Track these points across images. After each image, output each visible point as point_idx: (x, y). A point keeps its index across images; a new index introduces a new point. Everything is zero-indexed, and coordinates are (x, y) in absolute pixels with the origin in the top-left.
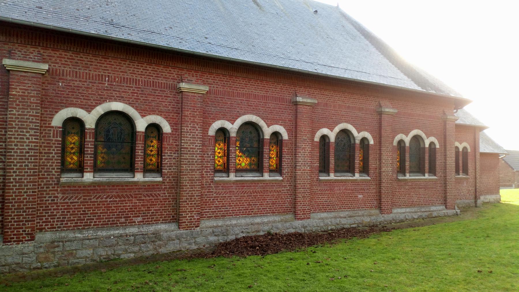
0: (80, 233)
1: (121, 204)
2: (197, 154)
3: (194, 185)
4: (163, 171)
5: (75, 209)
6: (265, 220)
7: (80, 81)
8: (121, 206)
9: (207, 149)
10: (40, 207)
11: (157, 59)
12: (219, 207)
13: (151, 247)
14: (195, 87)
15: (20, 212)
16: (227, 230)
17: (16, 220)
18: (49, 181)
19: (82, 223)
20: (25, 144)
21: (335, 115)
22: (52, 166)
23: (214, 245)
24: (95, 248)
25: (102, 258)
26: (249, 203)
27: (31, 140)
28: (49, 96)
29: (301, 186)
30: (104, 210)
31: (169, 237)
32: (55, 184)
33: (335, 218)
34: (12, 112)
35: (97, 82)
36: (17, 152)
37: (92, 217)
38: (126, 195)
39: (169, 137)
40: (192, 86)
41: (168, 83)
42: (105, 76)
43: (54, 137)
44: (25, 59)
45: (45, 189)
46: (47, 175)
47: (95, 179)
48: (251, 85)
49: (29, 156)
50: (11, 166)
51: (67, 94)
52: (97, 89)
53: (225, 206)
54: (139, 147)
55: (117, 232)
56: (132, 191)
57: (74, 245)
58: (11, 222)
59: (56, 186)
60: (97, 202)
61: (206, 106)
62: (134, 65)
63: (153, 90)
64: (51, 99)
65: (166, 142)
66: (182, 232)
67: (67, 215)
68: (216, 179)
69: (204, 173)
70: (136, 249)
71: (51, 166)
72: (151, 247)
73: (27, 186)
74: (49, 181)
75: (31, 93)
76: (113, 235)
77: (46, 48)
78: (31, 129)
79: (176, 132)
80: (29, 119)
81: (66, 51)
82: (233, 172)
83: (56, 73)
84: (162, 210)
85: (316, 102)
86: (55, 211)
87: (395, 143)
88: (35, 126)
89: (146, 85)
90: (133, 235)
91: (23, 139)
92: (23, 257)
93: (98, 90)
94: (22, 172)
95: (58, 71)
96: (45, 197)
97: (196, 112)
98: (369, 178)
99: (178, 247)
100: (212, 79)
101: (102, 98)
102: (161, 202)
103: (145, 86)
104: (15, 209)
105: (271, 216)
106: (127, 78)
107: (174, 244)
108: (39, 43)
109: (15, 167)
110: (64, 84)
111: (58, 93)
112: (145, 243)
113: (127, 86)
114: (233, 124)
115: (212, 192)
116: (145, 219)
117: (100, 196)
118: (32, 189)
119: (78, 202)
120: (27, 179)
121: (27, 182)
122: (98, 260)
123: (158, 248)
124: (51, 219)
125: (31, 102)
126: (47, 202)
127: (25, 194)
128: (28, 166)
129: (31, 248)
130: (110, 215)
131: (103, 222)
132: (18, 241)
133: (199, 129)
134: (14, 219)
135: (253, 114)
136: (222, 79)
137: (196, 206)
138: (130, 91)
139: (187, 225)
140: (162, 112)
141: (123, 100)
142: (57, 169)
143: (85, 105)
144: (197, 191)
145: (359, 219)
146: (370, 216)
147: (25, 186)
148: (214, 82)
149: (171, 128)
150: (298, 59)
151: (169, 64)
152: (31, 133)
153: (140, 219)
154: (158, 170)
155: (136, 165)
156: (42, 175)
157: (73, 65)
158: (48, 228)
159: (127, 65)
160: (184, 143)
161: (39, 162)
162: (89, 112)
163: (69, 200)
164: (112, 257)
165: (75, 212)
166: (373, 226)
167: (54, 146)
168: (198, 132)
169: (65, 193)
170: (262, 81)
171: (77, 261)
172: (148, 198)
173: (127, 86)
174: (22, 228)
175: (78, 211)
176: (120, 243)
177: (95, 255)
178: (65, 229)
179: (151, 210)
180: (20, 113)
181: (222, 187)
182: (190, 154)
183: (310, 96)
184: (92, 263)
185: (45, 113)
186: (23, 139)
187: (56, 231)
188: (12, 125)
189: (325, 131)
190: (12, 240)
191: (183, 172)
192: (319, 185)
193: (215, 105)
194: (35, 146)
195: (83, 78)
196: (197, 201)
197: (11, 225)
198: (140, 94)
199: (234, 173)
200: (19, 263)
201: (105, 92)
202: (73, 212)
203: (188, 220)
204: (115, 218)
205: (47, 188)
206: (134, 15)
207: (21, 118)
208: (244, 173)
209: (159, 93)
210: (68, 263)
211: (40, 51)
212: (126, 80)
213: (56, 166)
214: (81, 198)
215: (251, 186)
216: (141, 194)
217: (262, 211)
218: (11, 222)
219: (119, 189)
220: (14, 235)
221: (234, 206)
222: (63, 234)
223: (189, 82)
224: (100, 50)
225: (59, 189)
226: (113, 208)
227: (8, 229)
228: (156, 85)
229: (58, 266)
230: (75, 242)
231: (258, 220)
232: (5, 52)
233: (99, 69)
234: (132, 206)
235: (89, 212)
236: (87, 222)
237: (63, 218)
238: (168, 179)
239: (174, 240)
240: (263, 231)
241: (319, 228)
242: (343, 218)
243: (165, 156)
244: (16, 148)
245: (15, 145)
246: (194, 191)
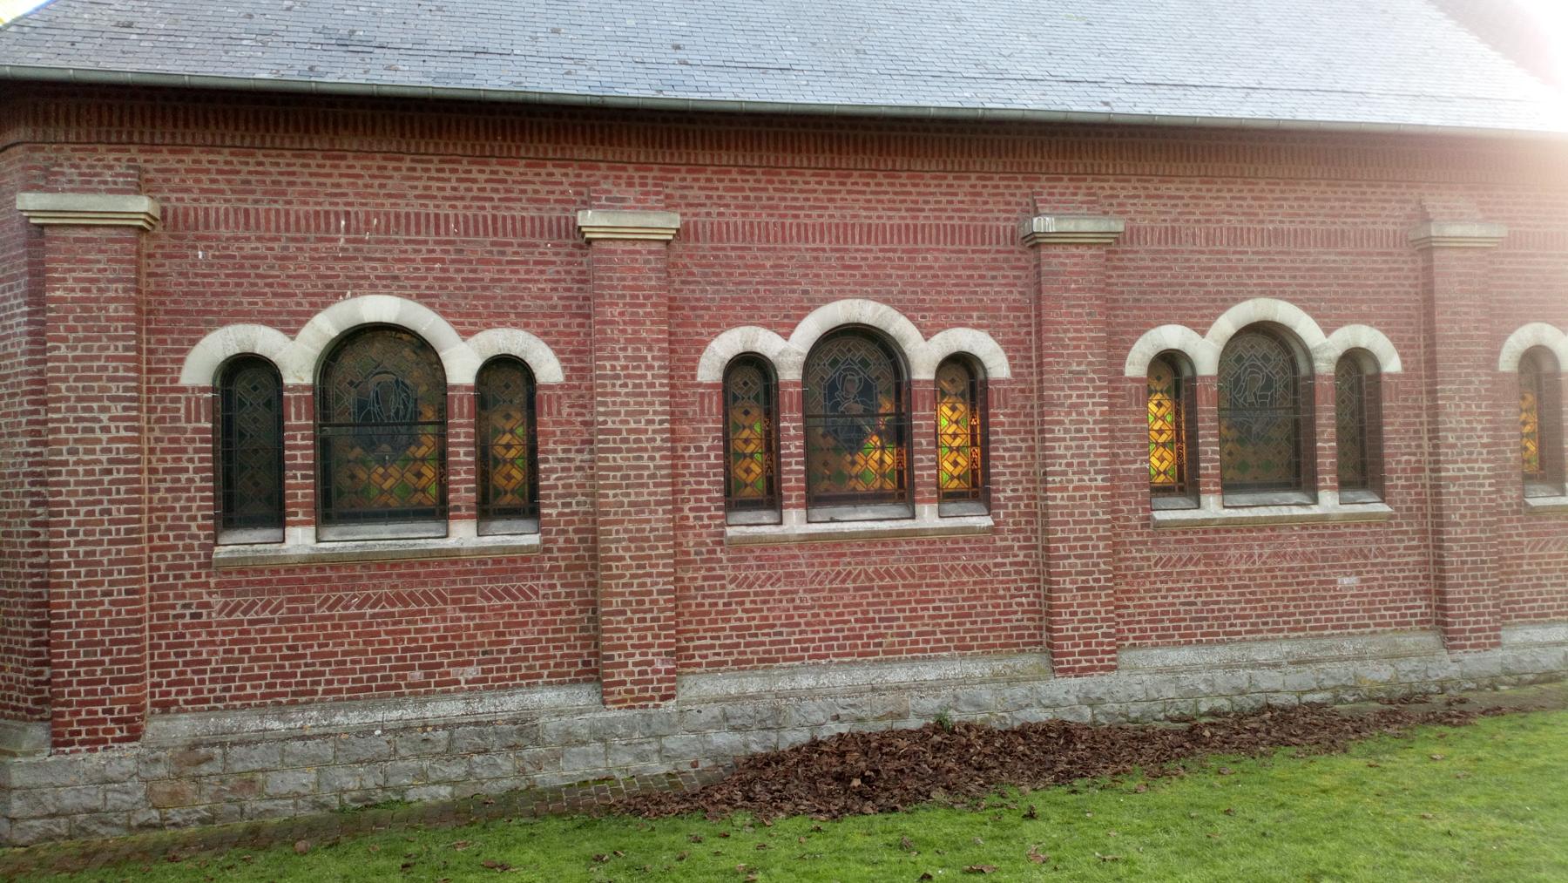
1: (408, 622)
2: (654, 449)
3: (649, 557)
4: (544, 511)
5: (263, 640)
6: (929, 673)
7: (259, 239)
8: (408, 632)
11: (504, 139)
12: (749, 628)
13: (506, 764)
14: (629, 220)
15: (95, 654)
17: (83, 677)
18: (182, 557)
19: (289, 685)
20: (98, 447)
21: (1213, 269)
22: (189, 509)
24: (322, 765)
25: (345, 797)
26: (865, 612)
27: (114, 433)
28: (170, 294)
29: (1072, 548)
32: (200, 566)
33: (1231, 666)
34: (56, 353)
35: (312, 236)
36: (75, 473)
37: (318, 668)
38: (424, 593)
39: (559, 397)
40: (627, 216)
41: (546, 216)
43: (188, 420)
44: (86, 187)
45: (171, 581)
46: (177, 538)
48: (849, 192)
49: (111, 482)
51: (223, 285)
52: (312, 259)
53: (773, 626)
55: (395, 714)
56: (444, 580)
57: (255, 759)
58: (69, 683)
59: (203, 572)
60: (332, 617)
62: (427, 170)
63: (493, 244)
64: (175, 302)
65: (550, 414)
66: (610, 715)
67: (242, 660)
68: (731, 532)
69: (686, 512)
70: (457, 770)
71: (183, 509)
72: (507, 766)
73: (110, 573)
74: (182, 557)
75: (107, 290)
76: (381, 725)
80: (105, 368)
81: (211, 147)
82: (797, 506)
83: (186, 221)
86: (204, 650)
87: (1507, 362)
88: (126, 389)
89: (471, 231)
90: (444, 727)
91: (92, 430)
92: (106, 791)
93: (316, 264)
94: (93, 533)
95: (192, 213)
96: (173, 607)
97: (643, 305)
98: (1384, 508)
100: (700, 188)
101: (330, 286)
102: (543, 614)
103: (467, 233)
104: (79, 645)
105: (953, 658)
106: (408, 215)
107: (587, 755)
108: (130, 134)
109: (73, 519)
110: (211, 253)
111: (196, 284)
112: (486, 751)
113: (407, 242)
114: (786, 336)
115: (723, 577)
116: (491, 671)
117: (340, 599)
118: (125, 582)
119: (272, 621)
120: (108, 552)
121: (111, 562)
122: (335, 804)
123: (529, 768)
124: (194, 672)
125: (108, 319)
127: (107, 599)
128: (109, 512)
129: (130, 765)
130: (374, 661)
131: (354, 681)
132: (93, 743)
133: (656, 364)
134: (78, 674)
136: (739, 184)
137: (660, 628)
138: (419, 257)
139: (631, 692)
140: (528, 316)
142: (204, 517)
143: (280, 313)
144: (660, 575)
145: (1339, 672)
146: (1393, 657)
147: (105, 573)
148: (709, 197)
150: (1036, 74)
151: (546, 152)
152: (114, 413)
153: (472, 672)
154: (528, 507)
155: (451, 496)
156: (161, 538)
157: (234, 192)
158: (186, 702)
159: (404, 173)
160: (605, 414)
161: (151, 501)
162: (292, 333)
163: (245, 613)
164: (379, 796)
166: (1406, 700)
167: (190, 448)
168: (655, 375)
169: (230, 594)
170: (892, 173)
171: (269, 805)
172: (496, 603)
176: (403, 752)
177: (326, 789)
178: (238, 703)
179: (510, 642)
180: (78, 353)
181: (758, 558)
182: (629, 450)
183: (1094, 206)
184: (318, 813)
186: (92, 430)
187: (210, 709)
188: (58, 390)
189: (1171, 336)
192: (1155, 542)
194: (127, 451)
195: (268, 229)
196: (662, 610)
198: (453, 261)
199: (802, 511)
200: (96, 810)
201: (338, 266)
202: (257, 650)
203: (632, 673)
204: (393, 669)
205: (176, 577)
207: (84, 369)
208: (844, 509)
210: (242, 812)
211: (134, 160)
212: (403, 221)
213: (199, 508)
214: (280, 606)
215: (867, 554)
216: (473, 591)
217: (916, 642)
218: (69, 683)
219: (400, 576)
221: (808, 624)
222: (228, 722)
223: (615, 203)
225: (212, 581)
226: (384, 637)
227: (63, 705)
229: (212, 820)
231: (900, 674)
232: (34, 172)
233: (316, 194)
234: (446, 629)
235: (308, 652)
236: (304, 684)
237: (229, 670)
238: (561, 539)
239: (584, 743)
240: (920, 716)
241: (1159, 707)
242: (1272, 668)
243: (546, 461)
244: (72, 459)
245: (72, 452)
246: (650, 575)
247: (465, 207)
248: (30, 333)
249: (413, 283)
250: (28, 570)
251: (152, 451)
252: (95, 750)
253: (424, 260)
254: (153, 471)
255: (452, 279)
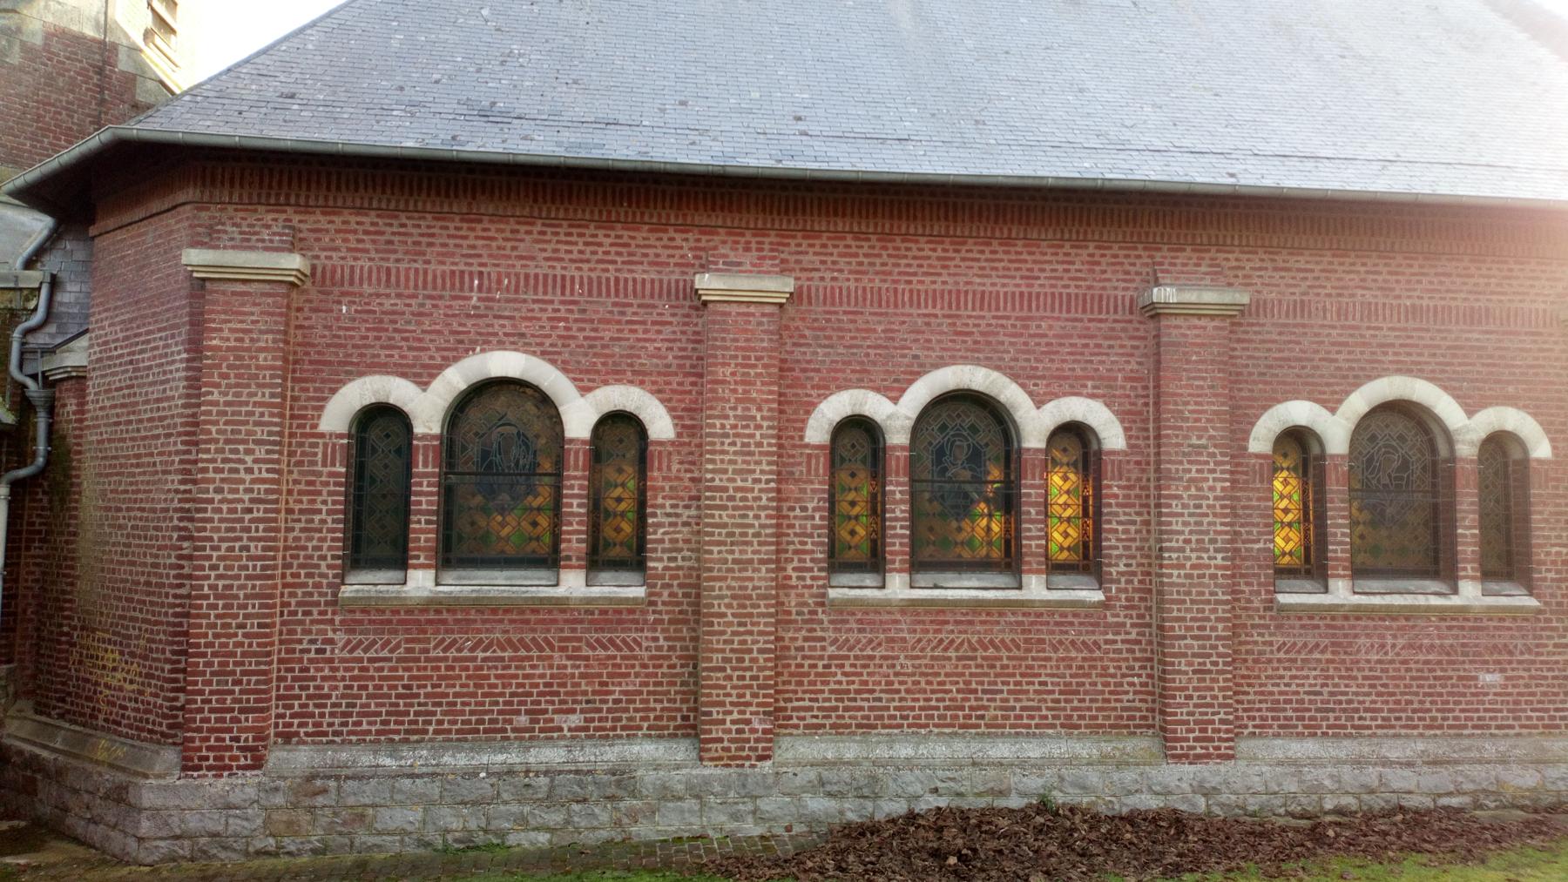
0: (391, 756)
1: (517, 668)
2: (760, 508)
3: (751, 615)
4: (651, 564)
5: (381, 678)
6: (1033, 750)
7: (399, 296)
8: (516, 676)
9: (803, 491)
10: (287, 670)
12: (848, 692)
13: (604, 815)
15: (218, 683)
16: (874, 779)
17: (214, 704)
18: (311, 594)
19: (402, 723)
20: (241, 487)
22: (319, 548)
23: (824, 829)
24: (429, 804)
25: (449, 837)
26: (967, 683)
27: (256, 475)
28: (313, 345)
29: (1188, 629)
30: (467, 686)
31: (665, 788)
32: (327, 604)
33: (1359, 762)
35: (447, 293)
36: (220, 510)
37: (430, 708)
39: (670, 453)
40: (742, 279)
41: (665, 278)
42: (471, 273)
43: (324, 464)
44: (245, 245)
45: (300, 616)
47: (440, 588)
48: (963, 259)
50: (204, 548)
52: (446, 315)
54: (572, 487)
55: (500, 758)
57: (367, 793)
58: (201, 710)
59: (330, 610)
60: (446, 659)
61: (795, 344)
62: (557, 234)
63: (615, 304)
64: (319, 353)
65: (660, 469)
66: (707, 772)
69: (790, 572)
70: (555, 818)
71: (316, 548)
72: (604, 817)
73: (245, 607)
74: (311, 594)
75: (258, 340)
76: (486, 768)
77: (306, 209)
78: (258, 442)
79: (693, 435)
80: (253, 414)
81: (360, 210)
82: (900, 571)
83: (333, 278)
84: (649, 693)
85: (1245, 299)
86: (326, 685)
90: (546, 773)
91: (237, 471)
93: (449, 320)
96: (300, 642)
97: (754, 366)
98: (1532, 602)
99: (696, 825)
100: (815, 254)
101: (461, 342)
102: (644, 666)
103: (590, 294)
104: (212, 674)
105: (1059, 736)
106: (536, 276)
107: (682, 812)
109: (215, 554)
110: (353, 308)
111: (339, 337)
112: (585, 800)
113: (535, 301)
114: (895, 400)
115: (823, 639)
116: (592, 720)
117: (454, 642)
124: (316, 706)
125: (258, 367)
126: (306, 656)
127: (240, 632)
128: (247, 549)
129: (251, 792)
130: (483, 704)
131: (463, 722)
132: (220, 769)
133: (765, 424)
134: (210, 701)
135: (977, 362)
136: (854, 250)
137: (759, 687)
138: (545, 316)
139: (728, 749)
140: (644, 373)
141: (526, 344)
142: (334, 557)
143: (414, 366)
144: (761, 633)
145: (1479, 776)
146: (1540, 762)
147: (240, 607)
149: (676, 425)
152: (258, 455)
153: (575, 720)
154: (635, 560)
155: (563, 546)
156: (293, 575)
158: (307, 734)
159: (535, 236)
160: (713, 471)
161: (286, 540)
162: (424, 385)
163: (366, 651)
164: (480, 839)
165: (381, 687)
167: (325, 490)
168: (763, 434)
169: (353, 632)
171: (377, 840)
172: (601, 652)
173: (535, 301)
174: (230, 730)
175: (391, 687)
176: (505, 796)
177: (430, 827)
178: (354, 738)
179: (612, 692)
180: (229, 398)
181: (860, 621)
182: (735, 508)
183: (1217, 277)
184: (421, 851)
185: (303, 395)
186: (237, 471)
189: (1300, 412)
190: (205, 764)
191: (711, 570)
192: (1277, 627)
193: (829, 338)
194: (267, 491)
195: (407, 287)
196: (761, 669)
197: (203, 720)
198: (576, 320)
199: (906, 576)
200: (217, 835)
201: (470, 322)
202: (375, 687)
203: (729, 731)
204: (500, 712)
206: (575, 82)
207: (233, 413)
208: (949, 575)
209: (635, 314)
212: (532, 282)
213: (330, 549)
214: (398, 646)
215: (971, 623)
216: (579, 640)
217: (1020, 717)
219: (512, 621)
220: (209, 749)
221: (908, 691)
223: (732, 267)
224: (456, 196)
225: (337, 618)
226: (493, 681)
227: (194, 731)
228: (626, 289)
229: (323, 851)
230: (373, 782)
231: (1002, 750)
232: (199, 230)
233: (453, 255)
234: (552, 676)
235: (422, 691)
236: (416, 722)
237: (348, 705)
238: (666, 593)
239: (680, 799)
240: (1022, 794)
241: (1278, 802)
244: (218, 497)
245: (219, 490)
246: (751, 633)
247: (590, 270)
248: (187, 379)
249: (538, 340)
250: (171, 600)
251: (290, 492)
252: (221, 776)
253: (550, 319)
254: (290, 511)
255: (574, 337)
